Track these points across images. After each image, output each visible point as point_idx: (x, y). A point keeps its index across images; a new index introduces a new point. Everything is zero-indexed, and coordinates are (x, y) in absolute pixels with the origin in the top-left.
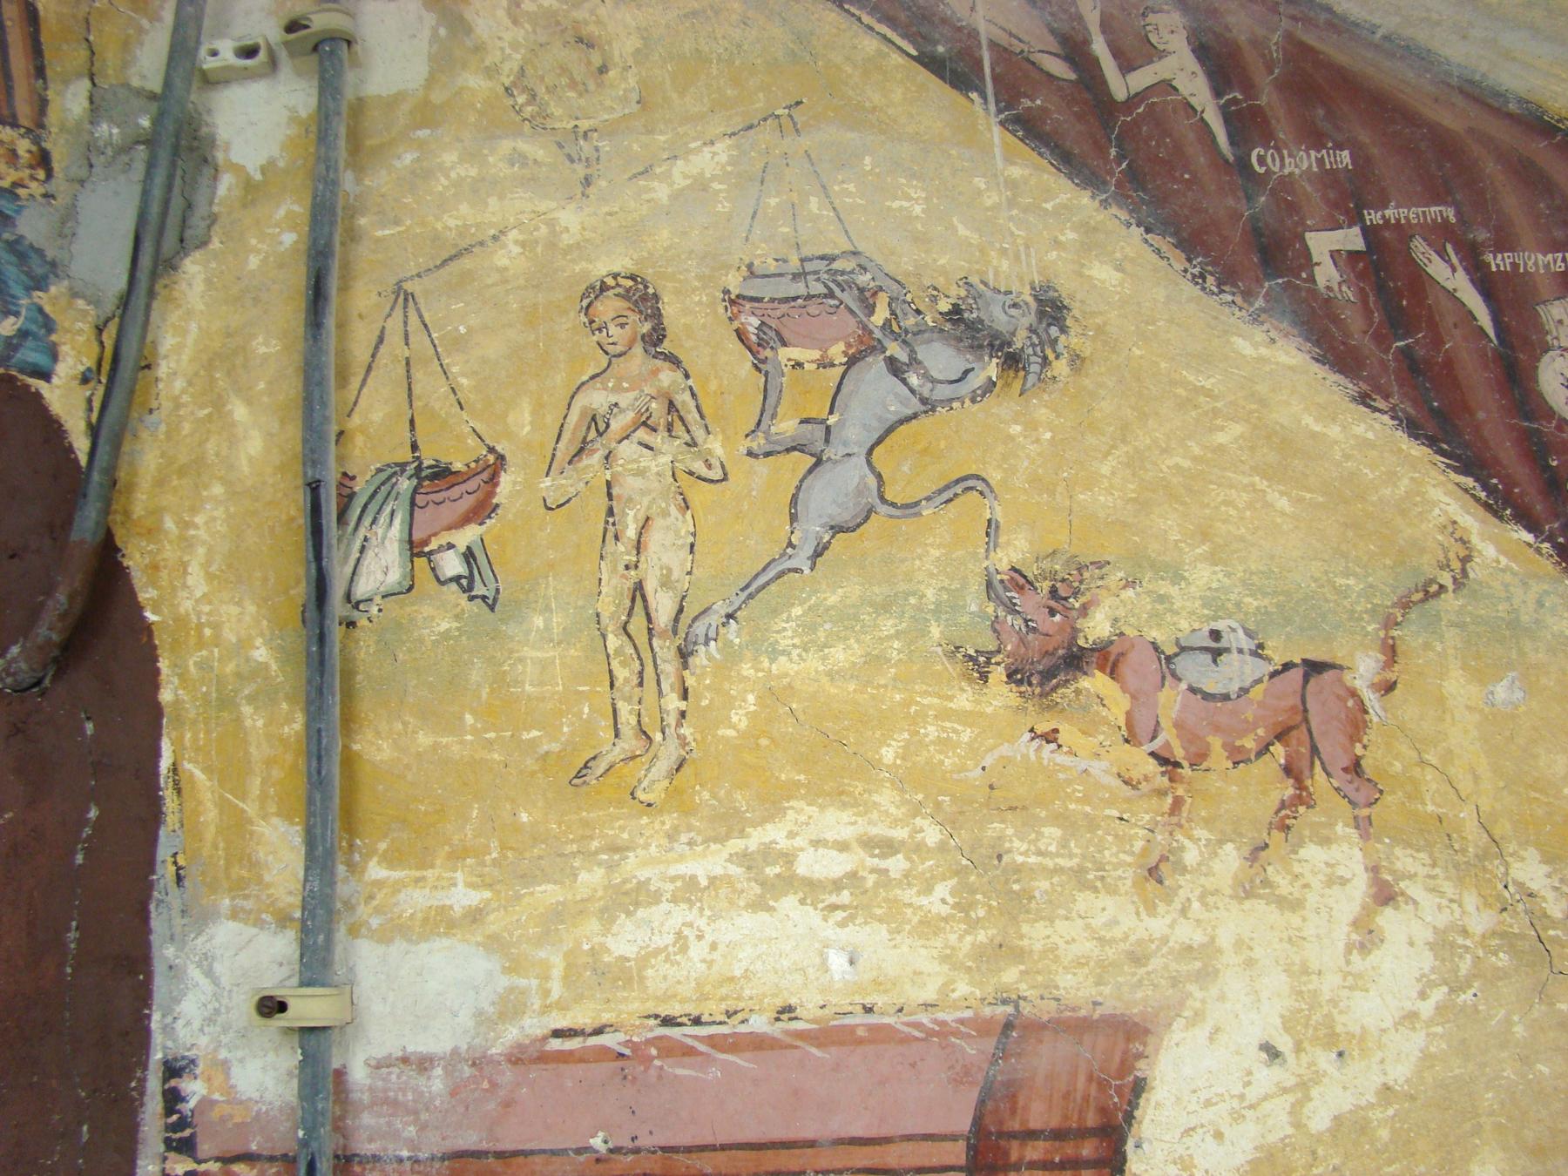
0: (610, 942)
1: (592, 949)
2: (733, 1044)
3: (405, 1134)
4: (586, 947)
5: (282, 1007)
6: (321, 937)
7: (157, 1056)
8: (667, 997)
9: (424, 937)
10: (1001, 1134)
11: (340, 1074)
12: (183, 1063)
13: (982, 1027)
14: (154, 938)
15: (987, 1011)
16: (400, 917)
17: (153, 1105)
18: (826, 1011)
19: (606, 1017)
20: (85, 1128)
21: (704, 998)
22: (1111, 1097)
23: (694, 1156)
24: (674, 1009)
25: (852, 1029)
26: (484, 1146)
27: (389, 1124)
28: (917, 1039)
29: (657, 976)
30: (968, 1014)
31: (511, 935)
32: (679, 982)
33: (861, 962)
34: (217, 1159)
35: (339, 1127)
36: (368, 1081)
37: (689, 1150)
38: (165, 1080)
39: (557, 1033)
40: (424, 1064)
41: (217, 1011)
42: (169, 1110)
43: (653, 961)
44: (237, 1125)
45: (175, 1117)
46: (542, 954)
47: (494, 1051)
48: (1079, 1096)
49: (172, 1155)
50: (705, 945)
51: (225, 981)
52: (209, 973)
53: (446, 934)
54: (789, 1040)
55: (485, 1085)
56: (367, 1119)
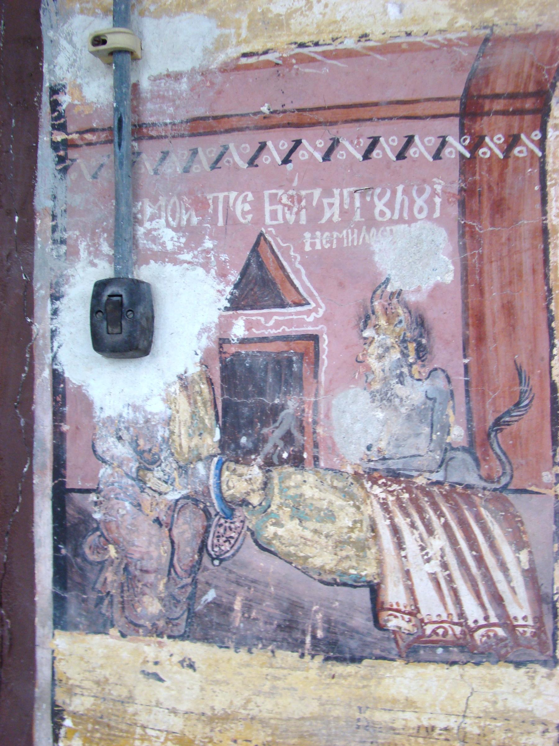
0: (272, 7)
1: (263, 11)
2: (336, 55)
3: (169, 112)
4: (259, 11)
5: (104, 42)
6: (123, 7)
7: (46, 85)
8: (301, 34)
9: (177, 14)
10: (479, 96)
11: (136, 86)
12: (59, 87)
13: (471, 41)
14: (43, 28)
15: (475, 33)
16: (165, 4)
17: (46, 108)
18: (386, 36)
19: (269, 45)
20: (13, 121)
21: (320, 32)
22: (544, 75)
23: (314, 113)
24: (305, 39)
25: (399, 45)
26: (208, 114)
27: (161, 108)
28: (435, 49)
29: (296, 23)
30: (464, 35)
31: (221, 9)
32: (308, 25)
33: (405, 10)
34: (77, 133)
35: (135, 110)
36: (150, 88)
37: (311, 110)
38: (51, 96)
39: (245, 55)
40: (177, 77)
41: (75, 61)
42: (53, 110)
43: (294, 15)
44: (86, 115)
45: (56, 114)
46: (237, 16)
47: (212, 67)
48: (525, 75)
49: (55, 132)
50: (321, 5)
51: (79, 46)
52: (71, 42)
53: (189, 12)
54: (364, 52)
55: (208, 84)
56: (150, 106)
